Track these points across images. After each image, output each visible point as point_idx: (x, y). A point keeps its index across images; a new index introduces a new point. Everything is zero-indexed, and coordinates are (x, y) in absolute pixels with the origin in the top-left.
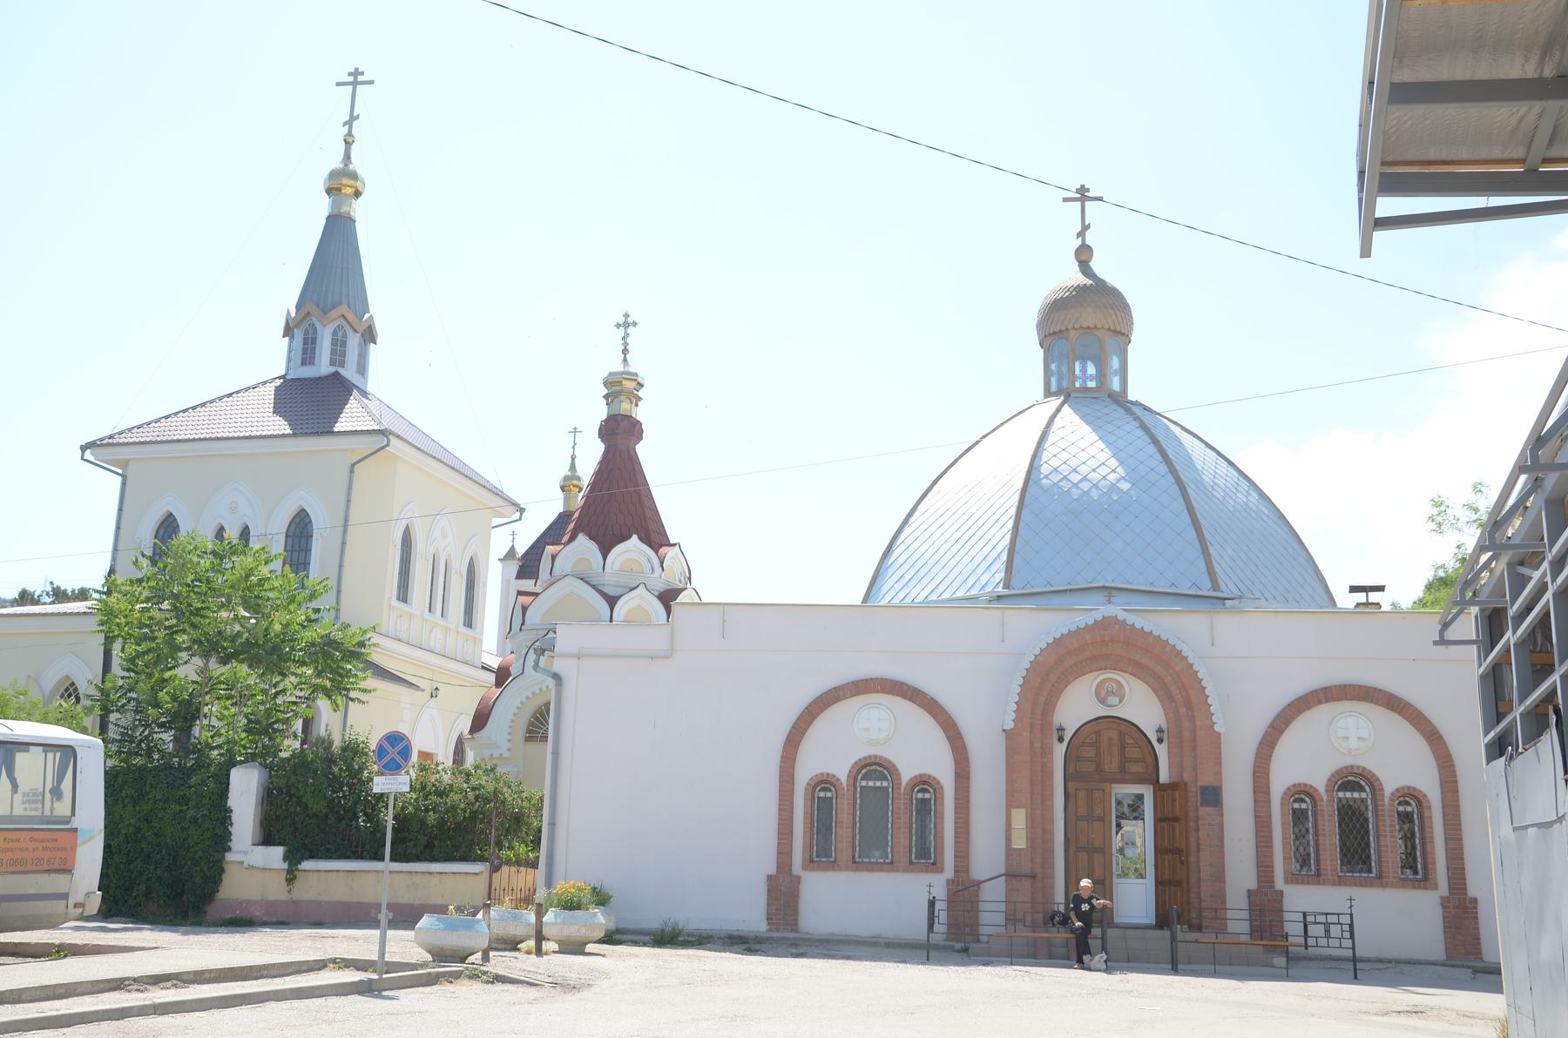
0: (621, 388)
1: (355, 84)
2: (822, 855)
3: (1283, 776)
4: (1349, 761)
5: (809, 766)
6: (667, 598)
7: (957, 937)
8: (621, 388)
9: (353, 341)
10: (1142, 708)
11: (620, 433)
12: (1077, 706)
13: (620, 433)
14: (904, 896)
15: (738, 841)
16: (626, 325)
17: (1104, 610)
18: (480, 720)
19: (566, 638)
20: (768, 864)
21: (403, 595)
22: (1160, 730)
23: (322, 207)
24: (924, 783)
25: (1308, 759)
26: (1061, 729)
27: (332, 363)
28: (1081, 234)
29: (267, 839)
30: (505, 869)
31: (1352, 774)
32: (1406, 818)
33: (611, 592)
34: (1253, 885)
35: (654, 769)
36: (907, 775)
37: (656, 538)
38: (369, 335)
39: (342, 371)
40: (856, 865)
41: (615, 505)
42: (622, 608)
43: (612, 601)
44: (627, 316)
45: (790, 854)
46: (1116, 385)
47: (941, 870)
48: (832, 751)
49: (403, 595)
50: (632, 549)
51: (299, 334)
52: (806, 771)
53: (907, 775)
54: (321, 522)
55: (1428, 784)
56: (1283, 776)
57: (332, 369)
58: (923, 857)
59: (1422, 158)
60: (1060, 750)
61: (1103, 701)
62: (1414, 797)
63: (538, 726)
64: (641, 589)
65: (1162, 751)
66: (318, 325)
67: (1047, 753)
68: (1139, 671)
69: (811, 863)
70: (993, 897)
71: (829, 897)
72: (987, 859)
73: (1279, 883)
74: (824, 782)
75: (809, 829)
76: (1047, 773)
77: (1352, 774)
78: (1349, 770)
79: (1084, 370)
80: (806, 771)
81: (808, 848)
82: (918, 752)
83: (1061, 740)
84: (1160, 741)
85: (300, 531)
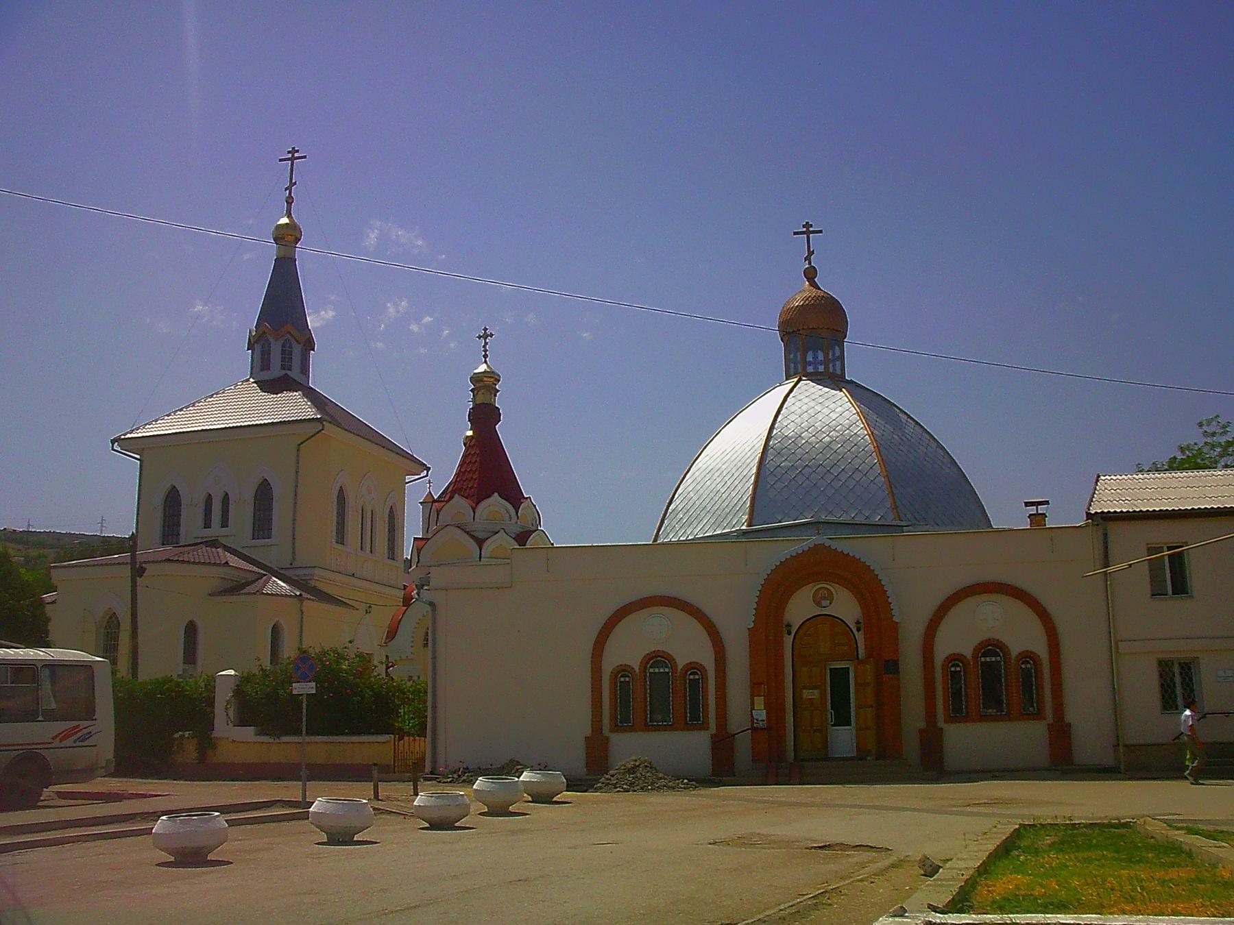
0: (485, 385)
1: (292, 159)
2: (623, 723)
3: (945, 646)
4: (987, 635)
5: (613, 658)
6: (522, 538)
7: (722, 769)
8: (485, 385)
9: (297, 350)
10: (846, 607)
11: (484, 416)
12: (800, 607)
13: (484, 416)
14: (694, 745)
15: (572, 716)
16: (485, 336)
17: (811, 540)
18: (392, 634)
19: (438, 577)
20: (584, 727)
21: (341, 540)
22: (858, 622)
23: (272, 250)
24: (694, 667)
25: (960, 636)
26: (789, 625)
27: (283, 368)
28: (808, 258)
29: (243, 723)
30: (406, 738)
31: (993, 645)
32: (1027, 674)
33: (481, 535)
34: (922, 724)
35: (508, 666)
36: (681, 663)
37: (514, 496)
38: (309, 345)
39: (289, 373)
40: (647, 728)
41: (487, 470)
42: (488, 547)
43: (480, 542)
44: (485, 329)
45: (600, 721)
46: (838, 372)
47: (707, 728)
48: (627, 650)
49: (341, 540)
50: (496, 502)
51: (258, 347)
52: (610, 663)
53: (681, 663)
54: (281, 492)
55: (1040, 647)
56: (945, 646)
57: (283, 372)
58: (693, 719)
59: (402, 459)
60: (788, 640)
61: (818, 604)
62: (1032, 658)
63: (428, 640)
64: (502, 533)
65: (860, 637)
66: (272, 340)
67: (779, 643)
68: (842, 581)
69: (616, 728)
70: (743, 747)
71: (627, 747)
72: (737, 719)
73: (941, 724)
74: (624, 670)
75: (614, 704)
76: (780, 656)
77: (993, 645)
78: (989, 642)
79: (815, 357)
80: (610, 663)
81: (613, 717)
82: (689, 647)
83: (789, 633)
84: (858, 630)
85: (264, 494)
